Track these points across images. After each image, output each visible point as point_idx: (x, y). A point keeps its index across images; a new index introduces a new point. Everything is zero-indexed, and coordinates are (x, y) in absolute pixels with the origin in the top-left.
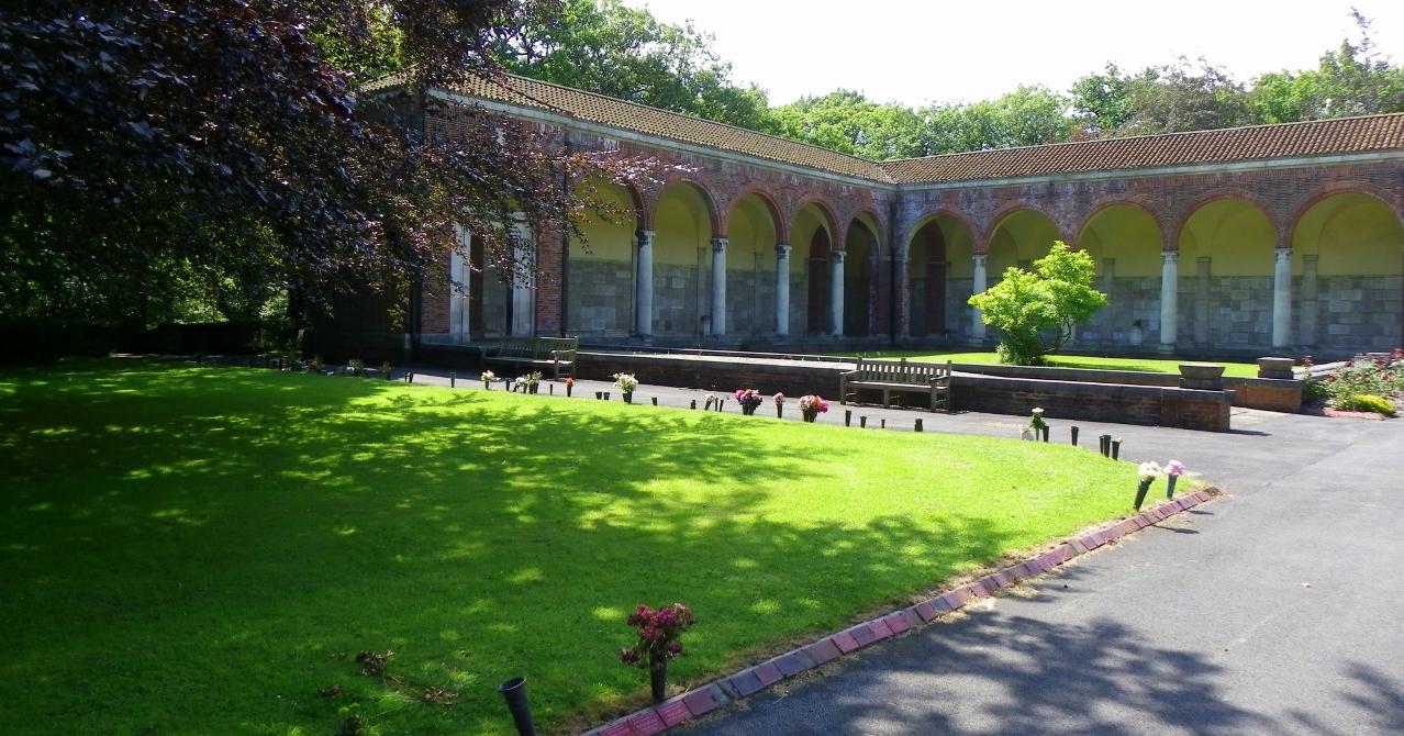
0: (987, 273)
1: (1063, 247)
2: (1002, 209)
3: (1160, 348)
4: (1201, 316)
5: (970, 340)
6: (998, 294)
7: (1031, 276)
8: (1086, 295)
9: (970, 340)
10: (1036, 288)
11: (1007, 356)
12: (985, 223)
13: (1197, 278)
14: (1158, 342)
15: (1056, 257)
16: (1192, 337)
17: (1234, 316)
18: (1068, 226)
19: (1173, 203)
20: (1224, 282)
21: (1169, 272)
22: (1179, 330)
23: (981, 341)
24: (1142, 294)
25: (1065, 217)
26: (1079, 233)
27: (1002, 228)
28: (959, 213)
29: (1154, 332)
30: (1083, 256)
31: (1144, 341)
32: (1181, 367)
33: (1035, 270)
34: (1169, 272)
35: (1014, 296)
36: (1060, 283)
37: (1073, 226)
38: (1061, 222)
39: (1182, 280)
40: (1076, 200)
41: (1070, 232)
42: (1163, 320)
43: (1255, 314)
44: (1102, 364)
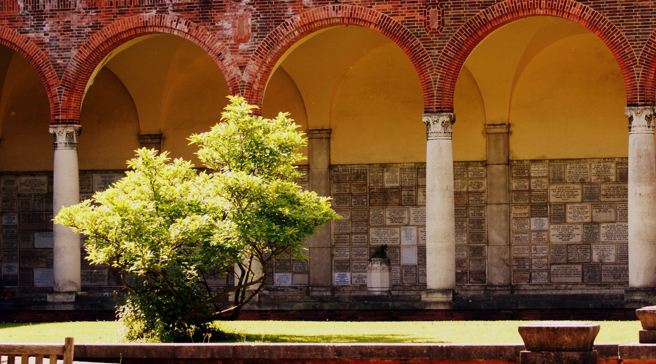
0: (80, 160)
1: (247, 108)
2: (109, 31)
3: (424, 297)
4: (496, 236)
5: (49, 298)
6: (122, 201)
7: (182, 166)
8: (293, 202)
9: (49, 298)
10: (193, 190)
11: (139, 326)
12: (72, 59)
13: (485, 164)
14: (424, 287)
15: (232, 127)
16: (480, 276)
17: (554, 234)
18: (242, 67)
19: (442, 23)
20: (535, 170)
21: (438, 154)
22: (459, 263)
23: (72, 298)
24: (385, 196)
25: (234, 49)
26: (262, 82)
27: (105, 69)
28: (18, 39)
29: (408, 268)
30: (284, 125)
31: (393, 287)
32: (522, 330)
33: (189, 153)
34: (438, 154)
35: (151, 206)
36: (244, 179)
37: (252, 67)
38: (228, 58)
39: (461, 167)
40: (255, 16)
41: (246, 77)
42: (430, 246)
43: (591, 227)
44: (326, 333)
